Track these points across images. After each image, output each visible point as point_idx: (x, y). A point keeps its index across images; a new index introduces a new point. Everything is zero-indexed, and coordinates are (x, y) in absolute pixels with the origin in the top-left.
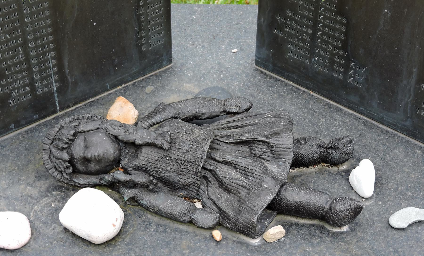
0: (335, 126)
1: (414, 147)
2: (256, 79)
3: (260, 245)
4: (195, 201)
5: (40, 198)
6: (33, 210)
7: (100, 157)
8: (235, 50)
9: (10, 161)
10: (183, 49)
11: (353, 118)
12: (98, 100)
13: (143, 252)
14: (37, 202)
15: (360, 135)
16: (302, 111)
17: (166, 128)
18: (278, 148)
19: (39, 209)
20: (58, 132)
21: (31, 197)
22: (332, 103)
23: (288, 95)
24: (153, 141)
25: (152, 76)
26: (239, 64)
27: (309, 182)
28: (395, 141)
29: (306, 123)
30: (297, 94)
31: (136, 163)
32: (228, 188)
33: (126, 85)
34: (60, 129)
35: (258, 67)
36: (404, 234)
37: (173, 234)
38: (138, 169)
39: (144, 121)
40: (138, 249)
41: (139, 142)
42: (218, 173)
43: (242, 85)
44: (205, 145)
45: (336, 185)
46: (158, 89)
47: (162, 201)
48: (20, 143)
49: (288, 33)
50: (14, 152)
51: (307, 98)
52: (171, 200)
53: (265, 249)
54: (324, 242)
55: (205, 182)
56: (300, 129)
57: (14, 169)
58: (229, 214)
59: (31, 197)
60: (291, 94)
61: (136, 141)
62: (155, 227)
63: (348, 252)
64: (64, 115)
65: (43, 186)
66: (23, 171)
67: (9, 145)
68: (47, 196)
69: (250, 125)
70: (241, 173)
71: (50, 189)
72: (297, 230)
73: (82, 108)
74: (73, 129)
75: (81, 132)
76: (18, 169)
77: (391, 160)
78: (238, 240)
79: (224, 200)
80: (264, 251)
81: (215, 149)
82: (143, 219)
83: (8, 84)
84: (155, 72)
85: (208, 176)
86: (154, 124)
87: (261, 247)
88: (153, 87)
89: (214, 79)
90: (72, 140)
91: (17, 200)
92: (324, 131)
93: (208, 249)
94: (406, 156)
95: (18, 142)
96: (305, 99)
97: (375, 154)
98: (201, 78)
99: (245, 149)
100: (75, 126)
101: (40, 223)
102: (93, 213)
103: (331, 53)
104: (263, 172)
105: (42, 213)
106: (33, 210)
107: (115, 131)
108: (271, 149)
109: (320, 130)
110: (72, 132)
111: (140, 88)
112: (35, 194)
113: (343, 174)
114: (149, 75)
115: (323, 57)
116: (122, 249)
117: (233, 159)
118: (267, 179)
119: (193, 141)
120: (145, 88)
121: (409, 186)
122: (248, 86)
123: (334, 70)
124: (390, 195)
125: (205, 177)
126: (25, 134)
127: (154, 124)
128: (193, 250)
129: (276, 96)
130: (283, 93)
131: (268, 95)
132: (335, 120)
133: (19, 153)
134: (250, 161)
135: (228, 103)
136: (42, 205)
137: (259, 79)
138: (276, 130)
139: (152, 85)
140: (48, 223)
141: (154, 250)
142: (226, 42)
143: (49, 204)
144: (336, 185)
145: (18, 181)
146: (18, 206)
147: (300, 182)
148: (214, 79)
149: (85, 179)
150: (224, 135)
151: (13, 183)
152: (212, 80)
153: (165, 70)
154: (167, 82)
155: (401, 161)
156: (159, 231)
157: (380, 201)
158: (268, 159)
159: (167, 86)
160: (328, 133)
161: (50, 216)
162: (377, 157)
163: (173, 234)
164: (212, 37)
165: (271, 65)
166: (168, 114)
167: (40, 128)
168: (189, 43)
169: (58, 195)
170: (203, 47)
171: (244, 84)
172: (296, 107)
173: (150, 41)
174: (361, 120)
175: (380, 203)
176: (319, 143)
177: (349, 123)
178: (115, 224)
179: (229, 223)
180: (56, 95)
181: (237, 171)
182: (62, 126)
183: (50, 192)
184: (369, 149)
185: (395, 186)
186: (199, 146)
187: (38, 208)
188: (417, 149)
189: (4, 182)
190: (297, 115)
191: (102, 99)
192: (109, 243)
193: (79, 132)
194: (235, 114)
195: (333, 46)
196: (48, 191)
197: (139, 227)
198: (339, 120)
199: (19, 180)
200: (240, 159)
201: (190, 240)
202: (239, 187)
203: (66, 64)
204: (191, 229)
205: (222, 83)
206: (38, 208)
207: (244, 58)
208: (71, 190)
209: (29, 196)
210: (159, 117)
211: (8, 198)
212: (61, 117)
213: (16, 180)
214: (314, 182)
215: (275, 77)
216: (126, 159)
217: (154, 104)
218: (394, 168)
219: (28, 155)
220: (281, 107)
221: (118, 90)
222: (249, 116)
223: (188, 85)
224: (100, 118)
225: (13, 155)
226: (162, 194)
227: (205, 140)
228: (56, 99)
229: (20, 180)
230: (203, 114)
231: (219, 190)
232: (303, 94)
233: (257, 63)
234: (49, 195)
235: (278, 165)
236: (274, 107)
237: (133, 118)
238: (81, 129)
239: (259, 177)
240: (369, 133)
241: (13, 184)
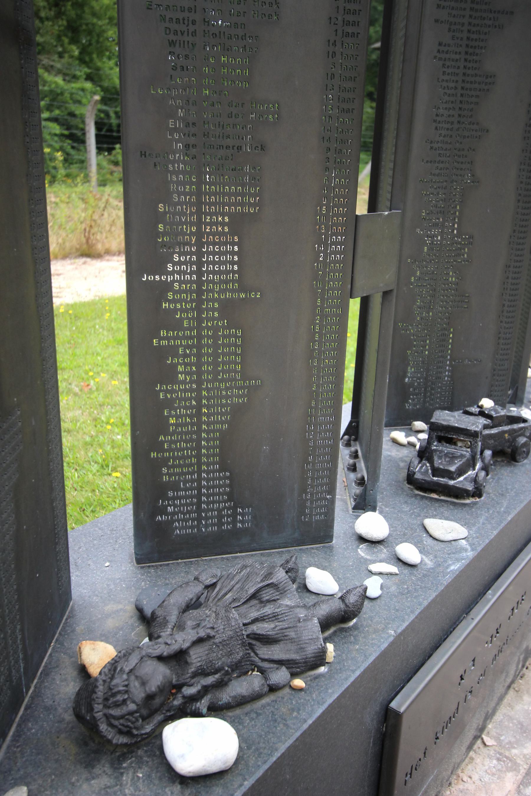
18: (280, 583)
19: (133, 790)
21: (109, 787)
31: (192, 669)
32: (276, 638)
38: (195, 675)
47: (240, 687)
57: (53, 780)
58: (295, 658)
59: (109, 787)
65: (106, 769)
68: (122, 774)
69: (236, 584)
76: (56, 776)
78: (312, 678)
94: (313, 557)
95: (18, 755)
99: (254, 602)
107: (157, 651)
108: (276, 588)
117: (259, 613)
120: (75, 631)
126: (14, 743)
143: (136, 778)
158: (278, 597)
161: (152, 785)
169: (131, 763)
179: (298, 668)
183: (121, 768)
199: (73, 784)
202: (284, 631)
206: (129, 789)
208: (136, 750)
209: (104, 789)
230: (191, 600)
234: (122, 771)
235: (288, 598)
239: (291, 613)
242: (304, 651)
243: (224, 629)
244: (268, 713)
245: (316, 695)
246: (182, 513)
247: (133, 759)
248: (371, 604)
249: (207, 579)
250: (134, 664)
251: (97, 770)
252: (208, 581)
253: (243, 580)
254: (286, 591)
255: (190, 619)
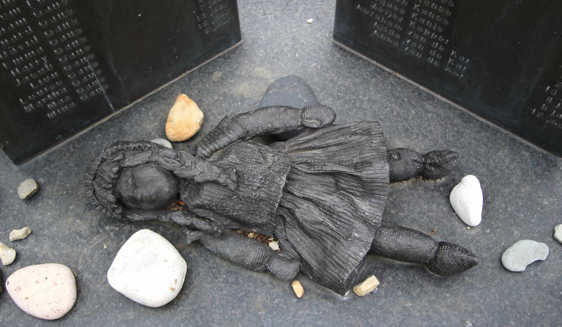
0: (427, 121)
1: (521, 147)
2: (335, 58)
3: (349, 299)
4: (270, 239)
5: (91, 236)
6: (82, 255)
7: (152, 197)
8: (310, 20)
9: (57, 182)
10: (253, 21)
11: (448, 108)
12: (159, 92)
13: (211, 314)
14: (87, 243)
15: (457, 132)
16: (389, 100)
17: (232, 158)
20: (99, 165)
21: (81, 236)
22: (422, 88)
23: (371, 78)
24: (215, 178)
25: (219, 57)
26: (317, 39)
27: (402, 202)
28: (498, 139)
29: (394, 116)
30: (382, 76)
33: (191, 71)
34: (102, 162)
35: (336, 42)
36: (521, 278)
37: (246, 285)
39: (205, 147)
40: (204, 310)
41: (198, 179)
42: (298, 214)
43: (319, 67)
44: (280, 181)
45: (434, 206)
46: (226, 75)
48: (70, 156)
49: (374, 10)
50: (62, 170)
51: (393, 83)
52: (242, 246)
53: (356, 306)
54: (426, 293)
55: (281, 220)
56: (388, 126)
57: (62, 195)
60: (375, 77)
61: (195, 178)
62: (225, 276)
63: (456, 308)
64: (121, 115)
66: (72, 197)
67: (58, 160)
68: (99, 233)
69: (334, 145)
70: (325, 213)
71: (102, 222)
72: (392, 275)
73: (141, 104)
74: (116, 166)
75: (126, 167)
76: (67, 193)
77: (496, 167)
79: (305, 247)
80: (355, 309)
81: (293, 180)
82: (210, 264)
83: (39, 98)
84: (223, 53)
85: (285, 216)
86: (216, 150)
87: (350, 303)
88: (220, 73)
89: (288, 59)
90: (118, 179)
91: (63, 240)
92: (415, 128)
93: (288, 309)
94: (513, 160)
95: (68, 155)
96: (391, 84)
97: (476, 159)
98: (274, 58)
100: (119, 161)
101: (89, 274)
102: (147, 266)
103: (428, 37)
104: (353, 215)
105: (92, 259)
106: (82, 255)
107: (169, 165)
109: (411, 127)
110: (115, 169)
111: (206, 75)
112: (85, 230)
113: (441, 189)
114: (217, 56)
115: (418, 42)
116: (185, 311)
117: (316, 196)
118: (358, 225)
119: (264, 166)
120: (212, 74)
121: (520, 204)
122: (326, 67)
123: (429, 56)
124: (498, 219)
125: (282, 217)
127: (216, 150)
128: (270, 309)
129: (358, 80)
130: (366, 77)
131: (349, 80)
132: (427, 111)
133: (69, 171)
134: (337, 200)
135: (308, 114)
136: (91, 247)
137: (338, 58)
138: (368, 157)
139: (220, 71)
140: (98, 274)
141: (224, 311)
142: (301, 8)
144: (434, 206)
145: (66, 211)
146: (64, 250)
147: (392, 203)
148: (288, 59)
149: (140, 215)
150: (303, 161)
151: (59, 216)
152: (287, 61)
153: (234, 49)
154: (236, 66)
155: (508, 167)
156: (230, 282)
157: (487, 228)
158: (358, 194)
159: (236, 71)
160: (419, 130)
162: (479, 163)
163: (246, 285)
164: (285, 4)
165: (351, 42)
166: (233, 135)
167: (94, 133)
168: (260, 13)
169: (112, 231)
170: (275, 16)
171: (322, 65)
172: (381, 95)
173: (213, 23)
174: (456, 111)
175: (488, 231)
176: (416, 158)
177: (443, 116)
178: (174, 288)
180: (107, 97)
181: (320, 210)
182: (104, 159)
183: (102, 227)
184: (469, 151)
185: (503, 205)
186: (272, 182)
187: (88, 251)
188: (525, 150)
189: (49, 214)
190: (383, 106)
191: (164, 90)
192: (170, 305)
193: (124, 167)
194: (314, 130)
195: (431, 30)
196: (100, 225)
197: (205, 277)
198: (431, 112)
199: (67, 210)
200: (323, 196)
201: (266, 294)
202: (323, 234)
203: (112, 64)
204: (266, 278)
205: (298, 65)
206: (88, 251)
207: (321, 30)
210: (223, 141)
211: (53, 238)
212: (118, 118)
213: (64, 210)
214: (408, 203)
215: (357, 55)
216: (187, 193)
217: (222, 96)
218: (500, 178)
219: (79, 173)
220: (365, 96)
221: (181, 78)
222: (332, 131)
223: (260, 69)
224: (150, 147)
225: (61, 174)
226: (230, 239)
227: (279, 172)
228: (108, 100)
229: (69, 209)
231: (299, 231)
232: (389, 77)
233: (335, 37)
235: (370, 201)
236: (357, 96)
237: (196, 123)
238: (127, 163)
240: (467, 128)
241: (59, 216)
242: (324, 269)
243: (259, 188)
244: (244, 288)
245: (303, 314)
246: (386, 18)
247: (117, 229)
248: (496, 272)
249: (310, 119)
250: (136, 163)
251: (89, 215)
252: (311, 121)
253: (346, 146)
254: (373, 194)
255: (237, 153)
